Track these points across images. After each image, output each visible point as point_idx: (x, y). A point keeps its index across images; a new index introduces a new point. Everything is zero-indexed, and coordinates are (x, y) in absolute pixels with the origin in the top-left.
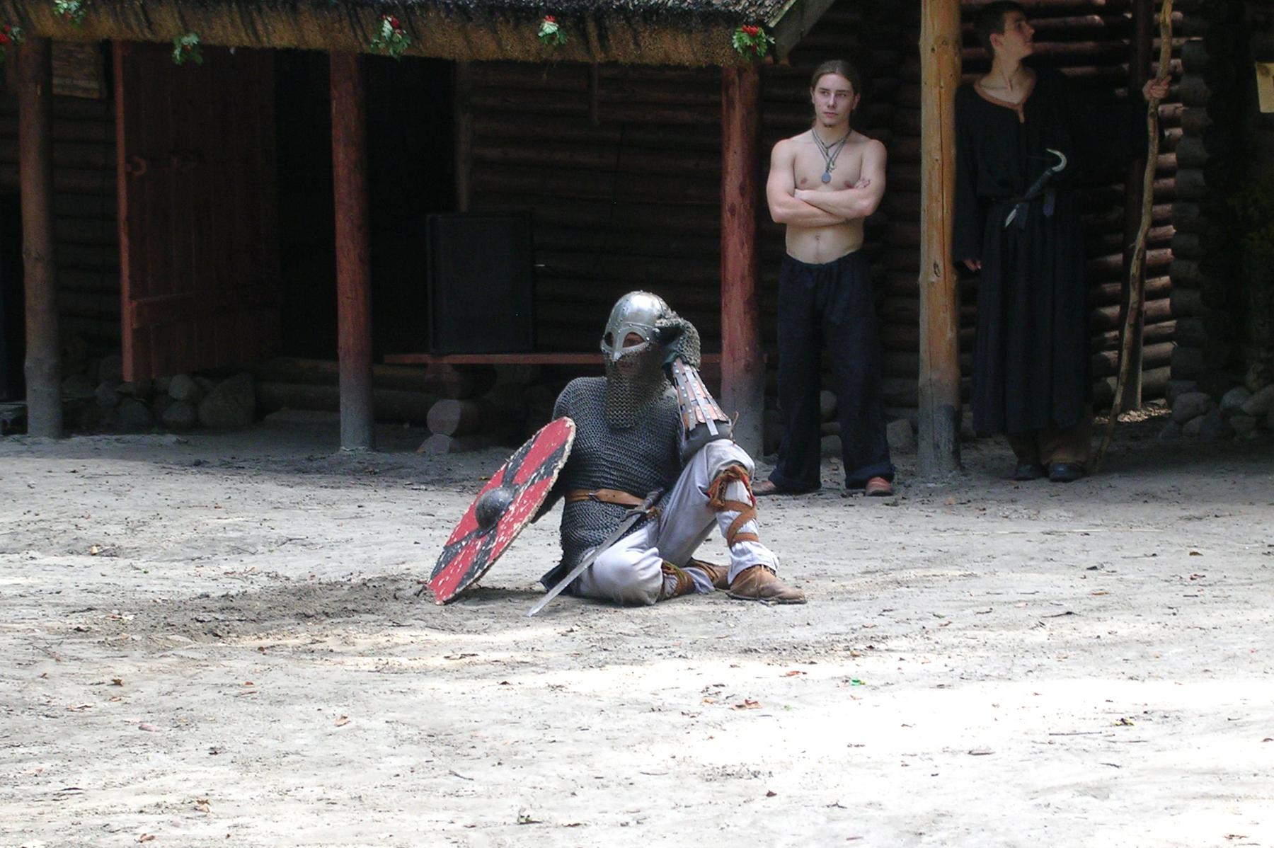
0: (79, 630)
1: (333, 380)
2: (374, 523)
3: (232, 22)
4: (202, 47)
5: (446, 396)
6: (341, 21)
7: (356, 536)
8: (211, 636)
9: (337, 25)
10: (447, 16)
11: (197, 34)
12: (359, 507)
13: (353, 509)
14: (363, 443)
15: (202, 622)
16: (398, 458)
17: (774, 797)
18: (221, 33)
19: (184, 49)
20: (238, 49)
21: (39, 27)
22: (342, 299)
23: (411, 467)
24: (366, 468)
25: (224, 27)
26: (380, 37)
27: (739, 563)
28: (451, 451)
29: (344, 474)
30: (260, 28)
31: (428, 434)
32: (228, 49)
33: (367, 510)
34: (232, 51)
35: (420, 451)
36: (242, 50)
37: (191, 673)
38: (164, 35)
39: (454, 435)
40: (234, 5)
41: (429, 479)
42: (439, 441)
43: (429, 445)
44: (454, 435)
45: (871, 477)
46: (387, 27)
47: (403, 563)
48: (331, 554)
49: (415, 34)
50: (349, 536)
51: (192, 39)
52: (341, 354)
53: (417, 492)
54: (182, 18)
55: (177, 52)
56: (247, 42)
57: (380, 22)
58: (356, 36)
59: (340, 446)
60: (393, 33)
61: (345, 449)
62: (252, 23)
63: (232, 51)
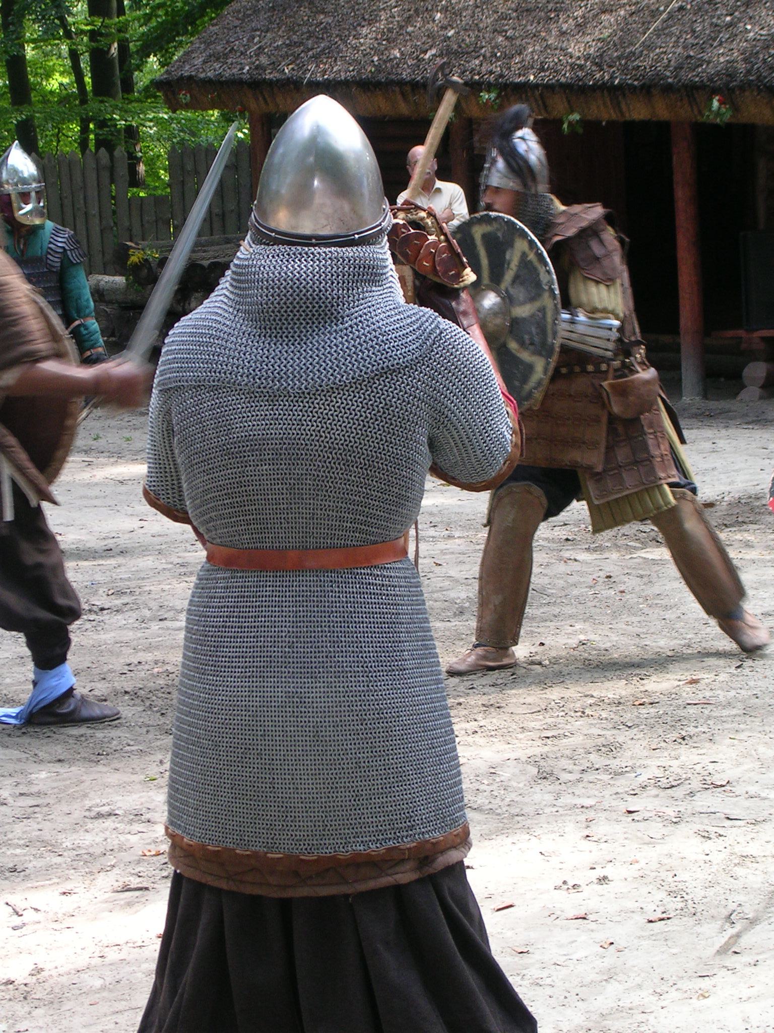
0: (567, 540)
1: (677, 349)
2: (727, 455)
3: (605, 104)
4: (583, 122)
5: (756, 359)
6: (681, 100)
7: (718, 465)
8: (654, 542)
9: (679, 104)
10: (758, 94)
11: (579, 112)
12: (714, 443)
13: (708, 445)
14: (698, 395)
15: (645, 532)
16: (723, 404)
17: (56, 507)
18: (596, 111)
19: (570, 124)
20: (608, 122)
21: (467, 112)
22: (682, 294)
23: (736, 411)
24: (703, 413)
25: (598, 107)
26: (710, 110)
27: (633, 366)
28: (761, 398)
29: (689, 418)
30: (623, 106)
31: (743, 387)
32: (601, 122)
33: (719, 446)
34: (604, 123)
35: (739, 398)
36: (610, 123)
37: (655, 569)
38: (555, 114)
39: (762, 387)
40: (605, 92)
41: (750, 419)
42: (751, 392)
43: (744, 395)
44: (762, 387)
45: (316, 88)
46: (716, 104)
47: (758, 485)
48: (705, 479)
49: (736, 108)
50: (713, 466)
51: (576, 117)
52: (682, 332)
53: (747, 431)
54: (569, 102)
55: (565, 126)
56: (614, 117)
57: (711, 100)
58: (692, 111)
59: (682, 396)
60: (719, 108)
61: (686, 400)
62: (619, 103)
63: (604, 123)
